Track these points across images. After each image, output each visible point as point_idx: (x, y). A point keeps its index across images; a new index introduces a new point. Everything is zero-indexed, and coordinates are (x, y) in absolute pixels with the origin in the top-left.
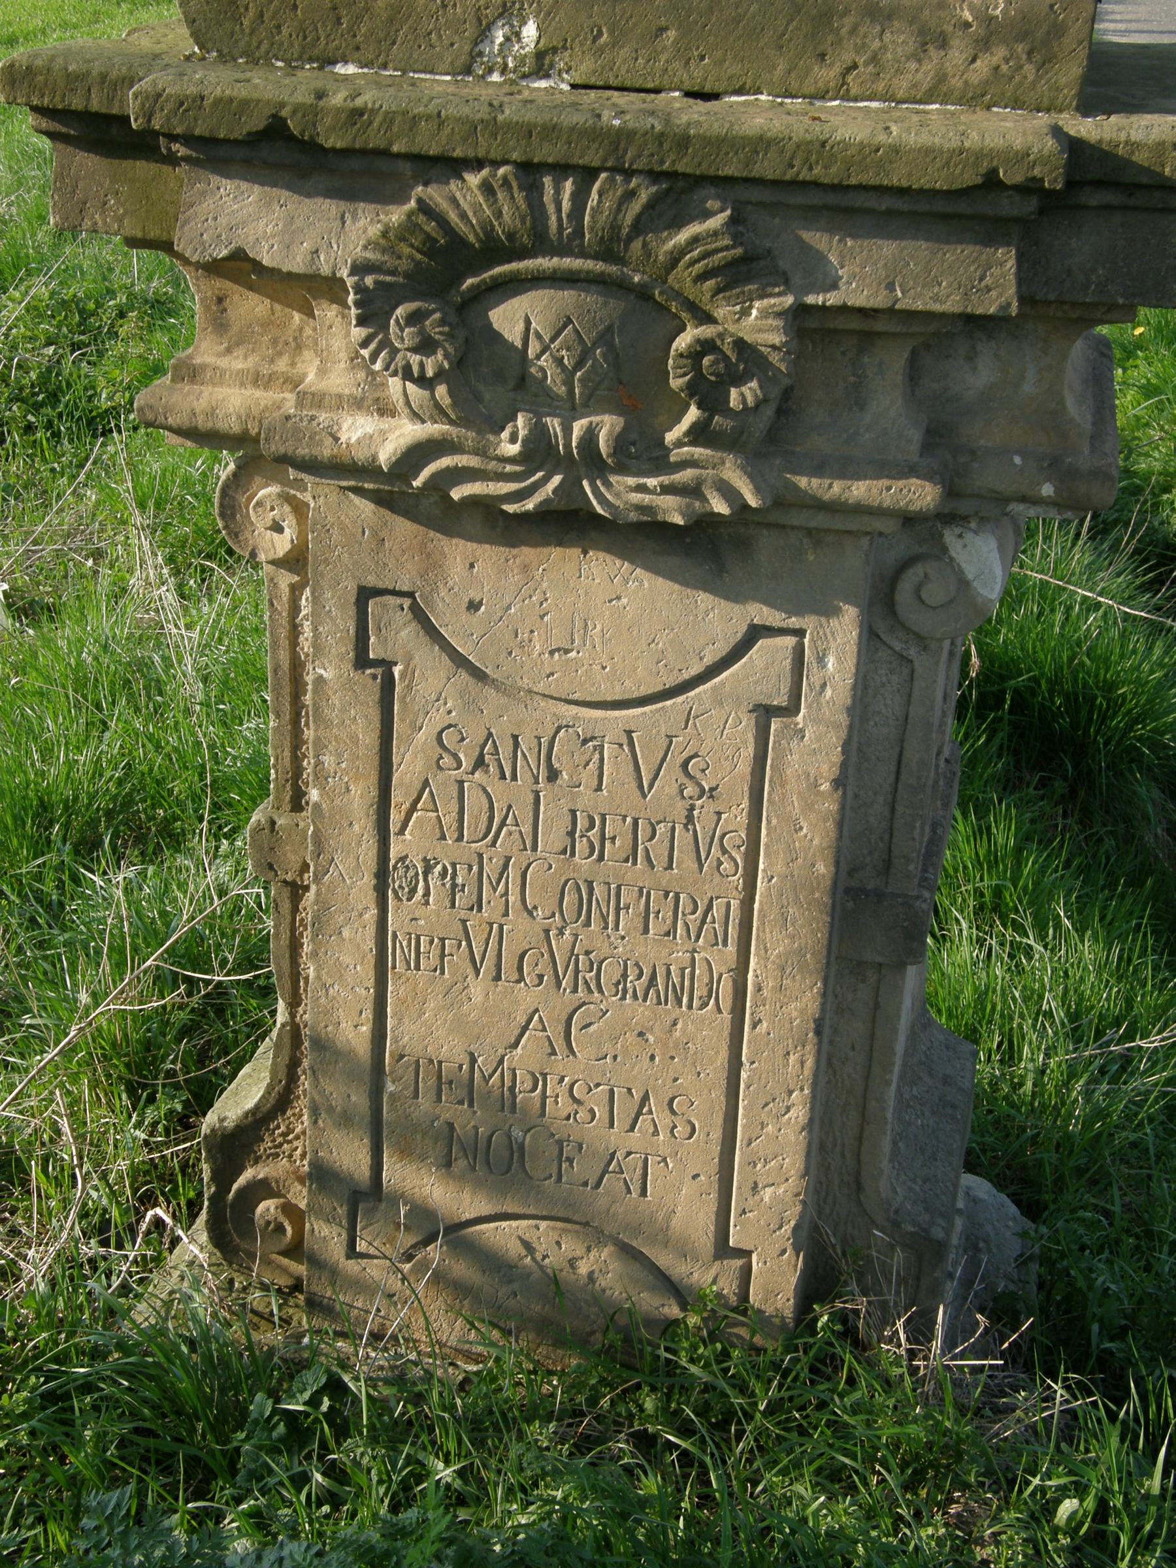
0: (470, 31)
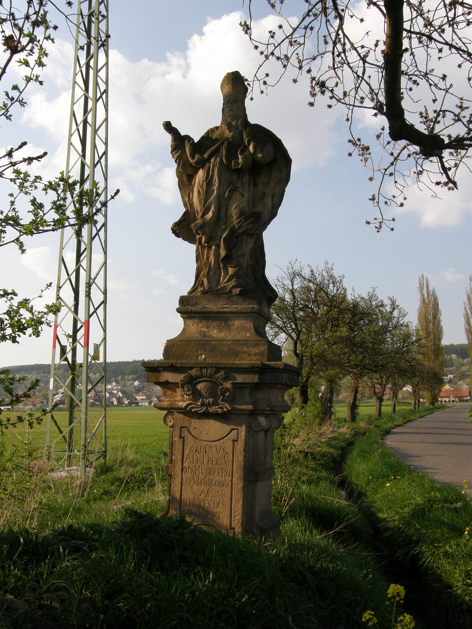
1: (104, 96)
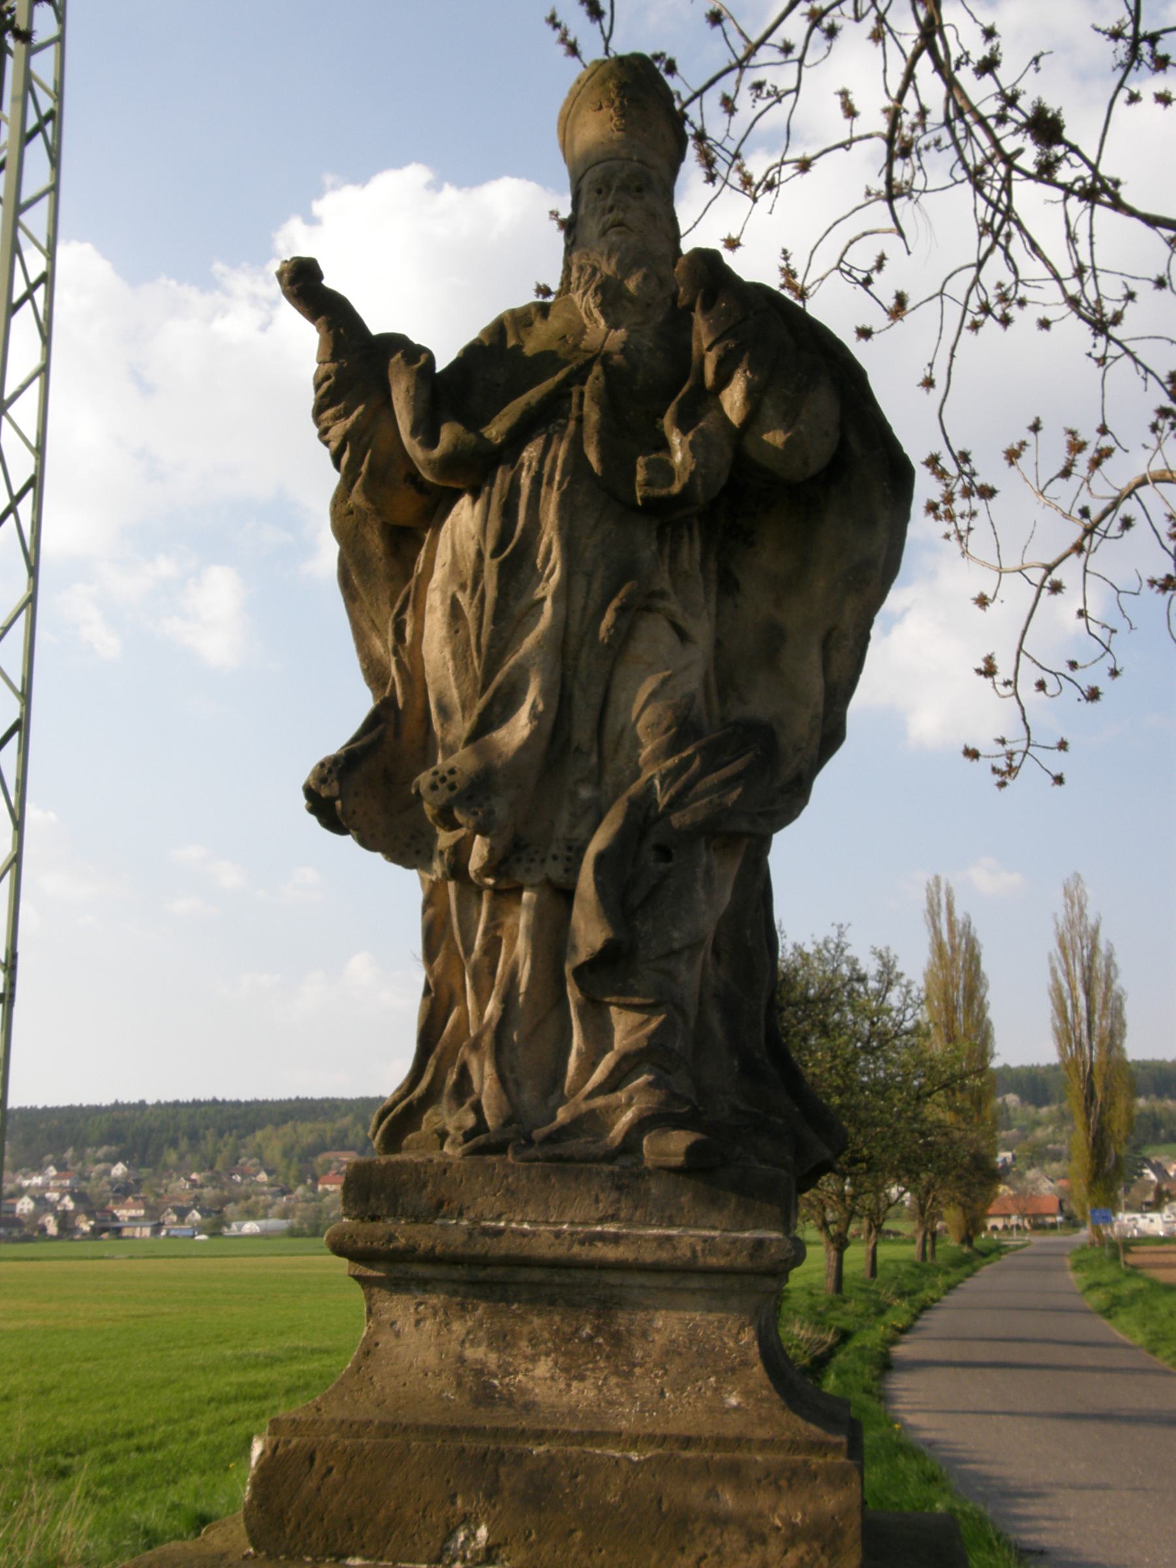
0: (441, 1533)
1: (40, 294)
